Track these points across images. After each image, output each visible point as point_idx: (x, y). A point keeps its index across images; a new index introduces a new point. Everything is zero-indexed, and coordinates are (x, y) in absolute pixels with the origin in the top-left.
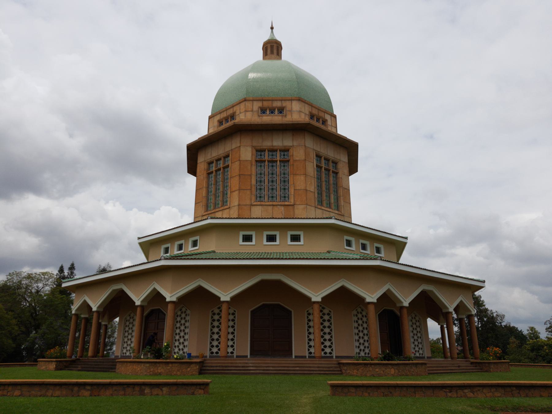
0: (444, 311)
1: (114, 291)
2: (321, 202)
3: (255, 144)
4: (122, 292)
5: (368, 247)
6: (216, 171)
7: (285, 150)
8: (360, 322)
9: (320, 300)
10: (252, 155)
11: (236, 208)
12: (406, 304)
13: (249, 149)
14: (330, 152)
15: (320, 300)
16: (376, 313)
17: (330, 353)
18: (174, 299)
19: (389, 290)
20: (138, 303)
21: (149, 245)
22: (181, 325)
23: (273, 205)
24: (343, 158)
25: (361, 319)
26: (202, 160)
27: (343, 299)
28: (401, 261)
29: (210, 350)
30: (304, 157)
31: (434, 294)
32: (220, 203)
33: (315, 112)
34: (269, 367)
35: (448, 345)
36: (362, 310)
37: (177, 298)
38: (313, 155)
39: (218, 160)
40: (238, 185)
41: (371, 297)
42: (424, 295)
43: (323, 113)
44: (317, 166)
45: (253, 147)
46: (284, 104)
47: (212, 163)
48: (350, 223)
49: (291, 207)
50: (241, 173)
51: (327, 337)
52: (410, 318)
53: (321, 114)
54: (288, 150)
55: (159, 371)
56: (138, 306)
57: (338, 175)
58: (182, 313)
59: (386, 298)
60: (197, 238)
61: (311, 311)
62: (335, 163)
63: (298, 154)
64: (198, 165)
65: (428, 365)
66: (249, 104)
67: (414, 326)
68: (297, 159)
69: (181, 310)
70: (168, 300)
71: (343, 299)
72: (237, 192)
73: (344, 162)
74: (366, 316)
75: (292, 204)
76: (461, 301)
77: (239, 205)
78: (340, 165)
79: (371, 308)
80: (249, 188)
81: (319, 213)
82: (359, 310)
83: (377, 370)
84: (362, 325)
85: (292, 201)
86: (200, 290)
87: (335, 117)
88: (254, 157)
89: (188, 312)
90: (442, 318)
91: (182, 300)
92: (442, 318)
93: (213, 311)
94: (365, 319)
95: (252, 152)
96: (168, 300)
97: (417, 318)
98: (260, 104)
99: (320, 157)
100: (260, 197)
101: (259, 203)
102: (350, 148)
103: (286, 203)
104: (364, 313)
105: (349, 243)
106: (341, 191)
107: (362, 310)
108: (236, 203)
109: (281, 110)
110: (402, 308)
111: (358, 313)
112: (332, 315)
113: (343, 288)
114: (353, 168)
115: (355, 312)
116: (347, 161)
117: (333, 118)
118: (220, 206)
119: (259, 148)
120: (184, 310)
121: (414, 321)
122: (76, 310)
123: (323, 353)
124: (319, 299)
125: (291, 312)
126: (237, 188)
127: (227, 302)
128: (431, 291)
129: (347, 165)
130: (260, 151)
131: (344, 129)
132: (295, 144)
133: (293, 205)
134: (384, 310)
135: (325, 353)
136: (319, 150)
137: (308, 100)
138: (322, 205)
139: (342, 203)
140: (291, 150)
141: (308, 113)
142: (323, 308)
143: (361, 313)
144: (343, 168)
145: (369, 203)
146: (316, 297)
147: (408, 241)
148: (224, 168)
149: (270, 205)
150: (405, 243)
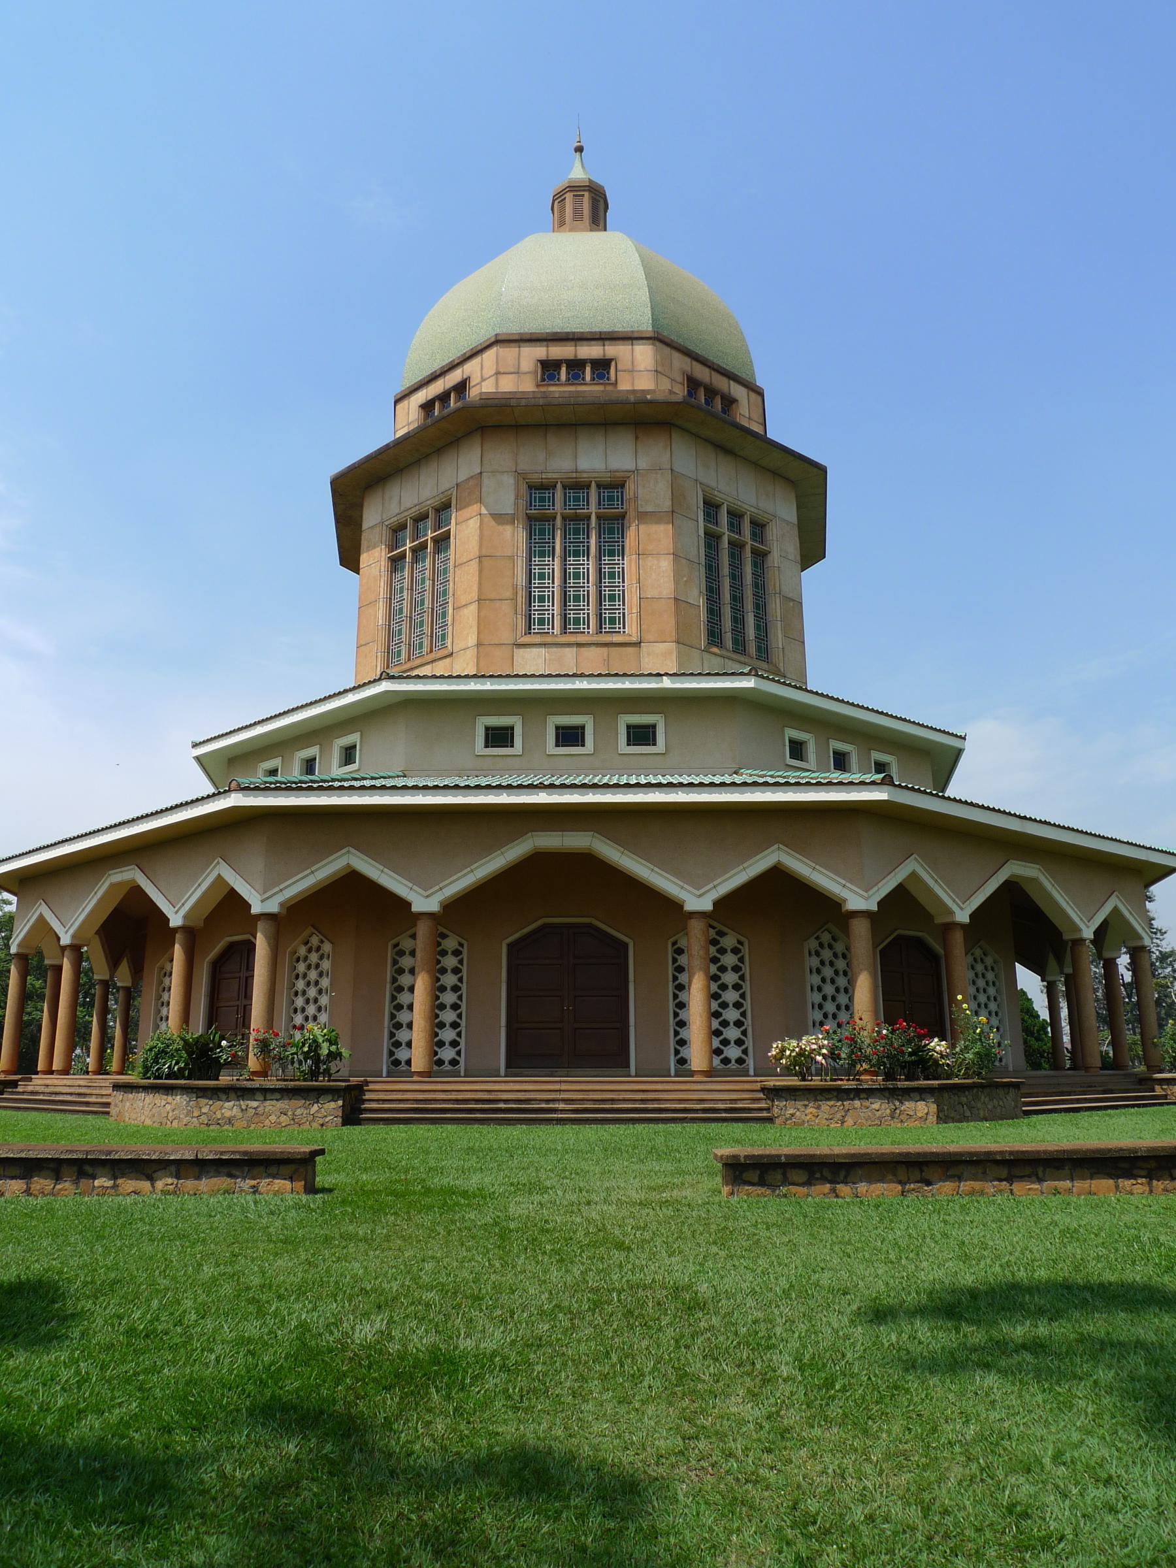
0: (1067, 936)
1: (112, 885)
2: (714, 636)
3: (525, 464)
4: (136, 892)
5: (854, 760)
6: (414, 550)
7: (614, 486)
8: (828, 972)
9: (708, 907)
10: (517, 498)
11: (471, 654)
12: (962, 916)
13: (509, 481)
14: (742, 490)
15: (708, 907)
16: (875, 946)
17: (740, 1061)
18: (273, 907)
19: (914, 874)
20: (176, 921)
21: (227, 764)
22: (308, 984)
23: (579, 645)
24: (783, 511)
25: (833, 981)
26: (377, 514)
27: (779, 911)
28: (950, 792)
29: (391, 1054)
30: (668, 503)
31: (1041, 885)
32: (426, 642)
33: (702, 373)
34: (553, 1100)
35: (1066, 1039)
36: (834, 939)
37: (281, 905)
38: (696, 502)
39: (421, 518)
40: (475, 588)
41: (859, 899)
42: (1012, 890)
43: (725, 380)
44: (707, 534)
45: (519, 475)
46: (611, 350)
47: (402, 527)
48: (800, 688)
49: (631, 650)
50: (484, 553)
51: (732, 1033)
52: (970, 959)
53: (721, 383)
54: (623, 486)
55: (228, 1114)
56: (176, 930)
57: (770, 558)
58: (310, 950)
59: (901, 901)
60: (353, 738)
61: (682, 943)
62: (759, 527)
63: (652, 492)
64: (364, 534)
65: (1023, 1090)
66: (508, 353)
67: (981, 983)
68: (650, 509)
69: (306, 943)
70: (256, 909)
71: (779, 911)
72: (473, 608)
73: (788, 523)
74: (844, 956)
75: (634, 639)
76: (1116, 910)
77: (479, 645)
78: (774, 532)
79: (861, 931)
80: (508, 594)
81: (715, 663)
82: (826, 938)
83: (876, 1106)
84: (833, 981)
85: (631, 630)
86: (352, 884)
87: (760, 393)
88: (522, 503)
89: (327, 947)
90: (1052, 963)
91: (459, 911)
92: (1052, 963)
93: (397, 945)
94: (841, 964)
95: (517, 489)
96: (256, 909)
97: (989, 961)
98: (540, 352)
99: (718, 506)
100: (541, 622)
101: (537, 639)
102: (804, 480)
103: (616, 639)
104: (839, 947)
105: (797, 749)
106: (775, 608)
107: (834, 939)
108: (472, 640)
109: (602, 366)
110: (952, 926)
111: (821, 945)
112: (745, 951)
113: (777, 874)
114: (812, 548)
115: (813, 944)
116: (794, 520)
117: (753, 395)
118: (425, 650)
119: (536, 478)
120: (315, 941)
121: (980, 968)
122: (19, 946)
123: (716, 1061)
124: (705, 904)
125: (626, 945)
126: (474, 595)
127: (431, 915)
128: (1034, 881)
129: (796, 532)
130: (539, 489)
131: (785, 427)
132: (643, 464)
133: (638, 644)
134: (899, 937)
135: (726, 1061)
136: (713, 484)
137: (680, 341)
138: (720, 644)
139: (778, 638)
140: (630, 487)
141: (679, 378)
142: (721, 934)
143: (830, 947)
144: (783, 544)
145: (857, 641)
146: (698, 900)
147: (968, 745)
148: (436, 541)
149: (569, 645)
150: (959, 752)
